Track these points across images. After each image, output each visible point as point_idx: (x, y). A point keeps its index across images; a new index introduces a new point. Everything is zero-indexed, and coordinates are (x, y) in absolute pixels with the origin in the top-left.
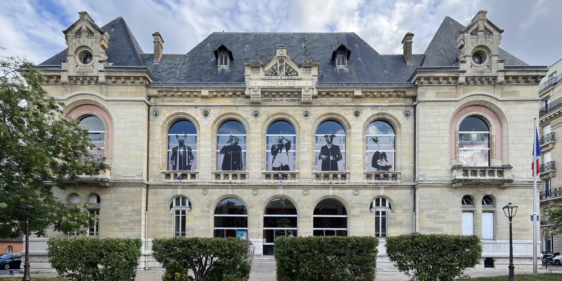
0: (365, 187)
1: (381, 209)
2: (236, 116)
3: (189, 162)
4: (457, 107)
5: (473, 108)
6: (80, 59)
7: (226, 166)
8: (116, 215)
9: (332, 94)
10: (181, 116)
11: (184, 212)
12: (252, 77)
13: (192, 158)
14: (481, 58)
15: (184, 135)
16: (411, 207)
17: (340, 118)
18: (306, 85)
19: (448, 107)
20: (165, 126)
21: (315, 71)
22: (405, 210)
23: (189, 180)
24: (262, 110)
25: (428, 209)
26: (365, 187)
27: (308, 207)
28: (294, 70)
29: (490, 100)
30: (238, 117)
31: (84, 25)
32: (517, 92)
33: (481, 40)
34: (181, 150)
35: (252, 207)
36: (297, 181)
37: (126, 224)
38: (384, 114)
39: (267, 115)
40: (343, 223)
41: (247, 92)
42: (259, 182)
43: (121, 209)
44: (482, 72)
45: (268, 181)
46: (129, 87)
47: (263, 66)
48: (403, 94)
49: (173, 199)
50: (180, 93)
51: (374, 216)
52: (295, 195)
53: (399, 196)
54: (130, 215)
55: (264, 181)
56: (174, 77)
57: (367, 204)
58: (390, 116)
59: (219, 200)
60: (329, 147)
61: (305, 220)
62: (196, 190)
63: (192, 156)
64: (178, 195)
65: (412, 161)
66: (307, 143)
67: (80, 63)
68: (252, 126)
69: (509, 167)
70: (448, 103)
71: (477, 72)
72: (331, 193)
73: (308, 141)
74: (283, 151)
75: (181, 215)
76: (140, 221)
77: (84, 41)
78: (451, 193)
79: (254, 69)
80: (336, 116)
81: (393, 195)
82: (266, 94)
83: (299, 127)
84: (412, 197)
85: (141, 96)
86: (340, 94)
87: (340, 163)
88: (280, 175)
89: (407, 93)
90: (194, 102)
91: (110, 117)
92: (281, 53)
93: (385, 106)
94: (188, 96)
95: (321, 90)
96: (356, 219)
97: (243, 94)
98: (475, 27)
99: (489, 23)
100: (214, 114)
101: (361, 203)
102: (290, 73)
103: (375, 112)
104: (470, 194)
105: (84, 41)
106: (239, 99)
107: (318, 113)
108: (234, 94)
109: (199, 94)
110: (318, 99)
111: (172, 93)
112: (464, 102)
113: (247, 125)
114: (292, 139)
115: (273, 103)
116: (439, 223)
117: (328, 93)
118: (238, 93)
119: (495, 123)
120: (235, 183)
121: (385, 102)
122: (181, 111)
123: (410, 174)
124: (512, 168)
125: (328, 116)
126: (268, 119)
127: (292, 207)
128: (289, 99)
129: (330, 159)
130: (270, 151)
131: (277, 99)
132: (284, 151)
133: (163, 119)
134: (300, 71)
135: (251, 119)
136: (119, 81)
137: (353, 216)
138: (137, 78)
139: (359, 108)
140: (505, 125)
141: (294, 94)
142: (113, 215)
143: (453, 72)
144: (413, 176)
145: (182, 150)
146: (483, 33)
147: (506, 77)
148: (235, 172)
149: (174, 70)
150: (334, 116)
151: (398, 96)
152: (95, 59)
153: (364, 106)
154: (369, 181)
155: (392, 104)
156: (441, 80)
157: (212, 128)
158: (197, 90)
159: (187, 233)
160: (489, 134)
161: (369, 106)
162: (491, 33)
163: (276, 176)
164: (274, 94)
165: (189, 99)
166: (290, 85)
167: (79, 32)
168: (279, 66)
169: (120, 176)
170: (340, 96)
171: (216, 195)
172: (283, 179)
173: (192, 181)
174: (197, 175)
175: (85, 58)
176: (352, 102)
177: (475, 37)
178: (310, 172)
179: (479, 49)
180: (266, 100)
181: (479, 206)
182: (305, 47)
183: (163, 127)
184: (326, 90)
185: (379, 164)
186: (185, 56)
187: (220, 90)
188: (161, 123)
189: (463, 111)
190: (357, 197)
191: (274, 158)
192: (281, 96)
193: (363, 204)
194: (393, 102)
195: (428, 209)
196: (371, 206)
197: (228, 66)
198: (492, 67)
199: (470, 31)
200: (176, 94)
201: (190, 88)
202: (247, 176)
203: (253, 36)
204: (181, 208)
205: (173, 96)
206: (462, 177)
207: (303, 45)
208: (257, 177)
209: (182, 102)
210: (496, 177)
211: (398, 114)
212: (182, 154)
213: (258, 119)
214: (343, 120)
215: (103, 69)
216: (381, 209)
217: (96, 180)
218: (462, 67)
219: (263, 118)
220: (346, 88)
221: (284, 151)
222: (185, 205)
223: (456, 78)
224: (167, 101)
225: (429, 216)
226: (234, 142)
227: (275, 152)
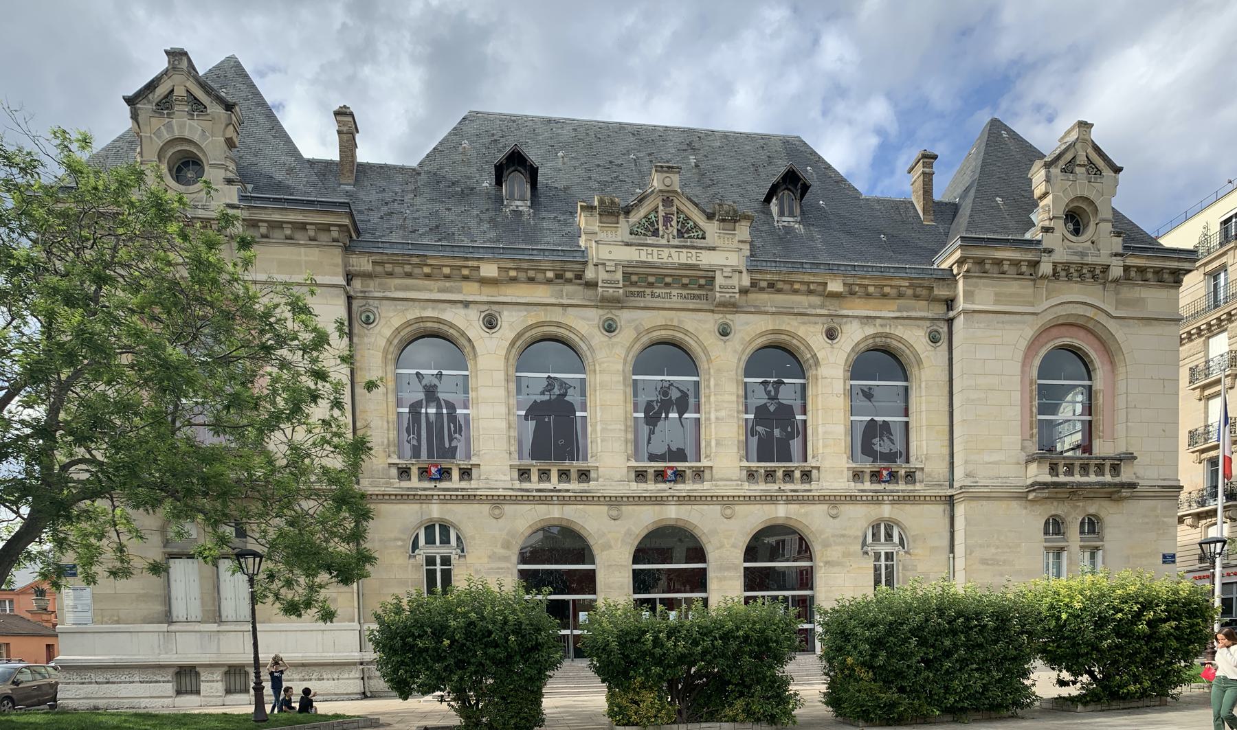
0: (852, 499)
3: (451, 439)
4: (1036, 328)
5: (1064, 330)
6: (170, 171)
7: (540, 450)
9: (780, 285)
10: (429, 325)
11: (446, 560)
12: (602, 236)
14: (1077, 224)
15: (435, 372)
16: (946, 542)
17: (795, 341)
20: (391, 349)
21: (743, 231)
22: (933, 550)
23: (455, 482)
24: (624, 317)
25: (981, 546)
26: (852, 499)
27: (734, 546)
28: (696, 225)
30: (567, 333)
33: (1081, 186)
34: (429, 411)
35: (607, 546)
36: (706, 485)
38: (887, 336)
39: (636, 328)
40: (806, 579)
41: (590, 274)
44: (1083, 255)
45: (643, 486)
46: (303, 250)
47: (627, 211)
49: (419, 528)
50: (427, 270)
51: (870, 563)
53: (921, 520)
55: (634, 485)
56: (403, 227)
57: (856, 537)
58: (901, 340)
59: (530, 531)
60: (772, 408)
63: (459, 426)
64: (431, 520)
65: (947, 443)
66: (727, 397)
68: (601, 355)
69: (1131, 457)
70: (1018, 317)
71: (1076, 254)
72: (781, 512)
73: (731, 394)
74: (671, 415)
75: (438, 568)
79: (604, 219)
80: (788, 338)
82: (634, 278)
83: (709, 360)
84: (947, 521)
85: (335, 274)
86: (796, 286)
87: (795, 444)
88: (669, 472)
89: (936, 292)
92: (668, 182)
94: (447, 277)
95: (758, 276)
96: (836, 569)
97: (579, 277)
98: (1069, 156)
99: (1097, 149)
100: (512, 323)
101: (843, 536)
102: (688, 231)
103: (870, 331)
104: (1059, 512)
105: (182, 126)
106: (569, 288)
107: (752, 329)
109: (475, 273)
110: (751, 296)
111: (408, 268)
112: (1049, 316)
113: (588, 353)
114: (692, 389)
115: (648, 301)
117: (771, 285)
118: (569, 275)
119: (1102, 363)
120: (567, 491)
121: (888, 310)
124: (1135, 458)
125: (770, 337)
126: (637, 339)
127: (578, 545)
128: (684, 292)
130: (642, 415)
132: (674, 415)
133: (388, 332)
134: (712, 229)
136: (277, 234)
137: (827, 563)
138: (326, 228)
139: (836, 320)
140: (1121, 370)
141: (699, 283)
144: (947, 475)
145: (432, 410)
147: (1127, 269)
150: (783, 337)
151: (916, 297)
153: (848, 316)
154: (860, 486)
155: (905, 314)
156: (1006, 267)
157: (507, 358)
158: (470, 263)
160: (1090, 387)
161: (857, 317)
162: (1098, 172)
163: (660, 476)
164: (651, 279)
165: (447, 284)
166: (690, 262)
168: (661, 213)
170: (796, 292)
171: (524, 521)
172: (675, 481)
173: (464, 484)
175: (179, 170)
176: (822, 307)
180: (633, 294)
181: (1074, 538)
182: (697, 166)
183: (386, 351)
184: (768, 277)
186: (415, 172)
187: (525, 265)
188: (382, 343)
189: (1044, 335)
190: (836, 521)
191: (652, 432)
192: (667, 285)
194: (907, 309)
195: (981, 546)
197: (529, 203)
198: (1102, 245)
199: (1062, 163)
200: (417, 271)
201: (454, 258)
202: (593, 474)
203: (568, 128)
205: (409, 275)
206: (1048, 478)
207: (692, 160)
208: (618, 477)
209: (431, 291)
210: (1108, 478)
211: (914, 338)
212: (432, 418)
214: (802, 348)
215: (236, 202)
216: (438, 550)
221: (674, 415)
223: (1035, 264)
226: (556, 391)
227: (653, 417)
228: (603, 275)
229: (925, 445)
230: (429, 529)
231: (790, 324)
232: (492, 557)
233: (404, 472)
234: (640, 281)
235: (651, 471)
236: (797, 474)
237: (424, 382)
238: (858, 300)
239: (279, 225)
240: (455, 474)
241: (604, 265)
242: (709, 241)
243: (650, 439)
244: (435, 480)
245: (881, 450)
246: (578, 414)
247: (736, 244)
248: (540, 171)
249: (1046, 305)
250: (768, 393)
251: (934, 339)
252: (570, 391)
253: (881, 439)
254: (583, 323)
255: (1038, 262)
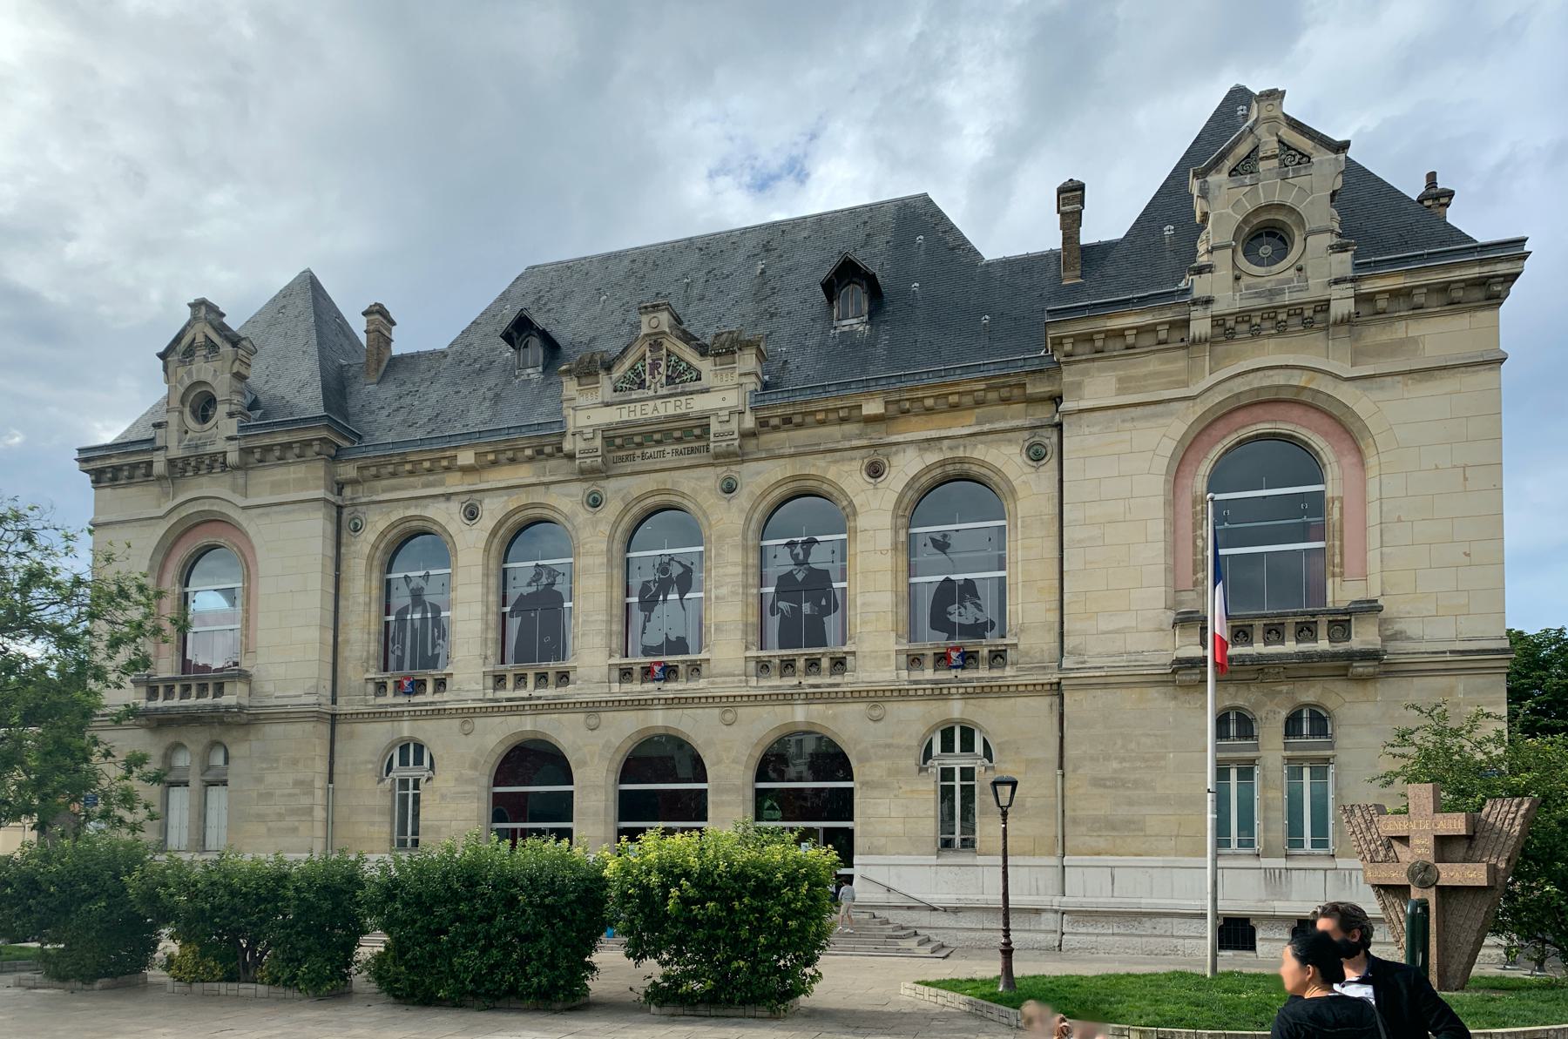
0: (903, 694)
1: (957, 762)
2: (414, 523)
3: (434, 646)
8: (260, 795)
10: (414, 523)
12: (581, 401)
13: (443, 634)
18: (724, 404)
19: (1161, 421)
23: (429, 696)
24: (610, 487)
25: (1092, 759)
28: (689, 366)
29: (1311, 380)
31: (202, 331)
32: (1414, 340)
35: (583, 763)
36: (702, 683)
37: (280, 816)
38: (962, 461)
42: (601, 694)
43: (271, 778)
44: (1272, 293)
47: (608, 368)
48: (1016, 392)
49: (393, 747)
50: (408, 467)
52: (695, 726)
54: (290, 795)
55: (616, 687)
57: (909, 748)
58: (983, 464)
60: (800, 577)
61: (724, 798)
62: (566, 718)
63: (440, 628)
64: (402, 739)
67: (191, 423)
70: (1159, 408)
71: (1258, 295)
73: (735, 564)
74: (670, 597)
76: (310, 811)
77: (198, 371)
78: (1172, 704)
79: (584, 381)
81: (990, 717)
85: (317, 488)
87: (831, 623)
88: (657, 669)
89: (1030, 390)
90: (442, 484)
91: (252, 547)
92: (654, 323)
93: (961, 437)
94: (430, 471)
95: (766, 413)
96: (876, 793)
97: (560, 450)
100: (907, 466)
101: (889, 746)
103: (932, 457)
104: (1240, 702)
105: (198, 371)
106: (552, 463)
107: (762, 477)
108: (540, 452)
110: (764, 438)
112: (1217, 397)
115: (639, 464)
116: (1131, 803)
117: (787, 420)
118: (548, 450)
122: (412, 512)
123: (1045, 647)
126: (626, 510)
128: (679, 447)
129: (802, 611)
131: (649, 451)
134: (705, 366)
135: (583, 515)
139: (881, 450)
141: (691, 434)
142: (255, 795)
143: (1170, 307)
145: (417, 616)
146: (1275, 162)
147: (1360, 298)
148: (544, 666)
149: (408, 400)
152: (222, 409)
155: (986, 427)
157: (487, 550)
158: (448, 454)
159: (421, 839)
161: (912, 442)
162: (1305, 158)
163: (647, 673)
165: (431, 478)
166: (679, 411)
167: (190, 352)
168: (648, 361)
169: (268, 696)
170: (822, 423)
171: (496, 735)
172: (666, 680)
174: (448, 682)
176: (859, 436)
177: (1248, 179)
178: (742, 654)
179: (1265, 217)
180: (621, 459)
183: (370, 558)
184: (780, 411)
185: (955, 618)
187: (501, 447)
188: (367, 549)
190: (734, 727)
192: (659, 442)
193: (898, 747)
195: (1092, 759)
196: (928, 754)
199: (1229, 163)
203: (626, 262)
204: (411, 772)
205: (394, 475)
208: (597, 677)
210: (1323, 645)
211: (1005, 459)
212: (417, 624)
213: (600, 515)
216: (957, 762)
217: (216, 708)
218: (1200, 286)
219: (611, 509)
220: (836, 398)
222: (952, 750)
224: (382, 491)
225: (1098, 782)
226: (544, 581)
228: (581, 445)
229: (1028, 614)
230: (404, 749)
231: (815, 466)
232: (459, 780)
233: (381, 687)
234: (622, 444)
235: (637, 668)
236: (825, 663)
237: (412, 585)
238: (914, 419)
239: (268, 449)
240: (430, 687)
241: (581, 433)
242: (704, 383)
243: (644, 628)
244: (409, 694)
245: (957, 626)
246: (566, 605)
247: (736, 379)
248: (956, 208)
249: (1210, 380)
250: (795, 557)
251: (1036, 455)
252: (559, 579)
253: (961, 604)
254: (566, 501)
255: (1188, 321)
